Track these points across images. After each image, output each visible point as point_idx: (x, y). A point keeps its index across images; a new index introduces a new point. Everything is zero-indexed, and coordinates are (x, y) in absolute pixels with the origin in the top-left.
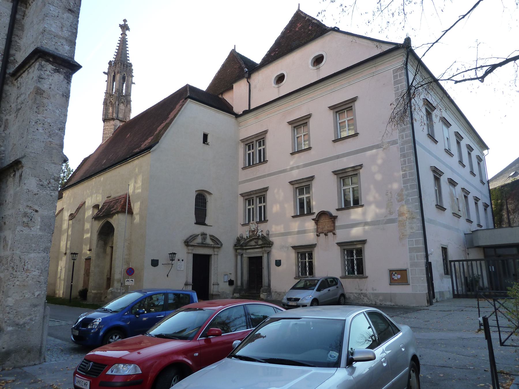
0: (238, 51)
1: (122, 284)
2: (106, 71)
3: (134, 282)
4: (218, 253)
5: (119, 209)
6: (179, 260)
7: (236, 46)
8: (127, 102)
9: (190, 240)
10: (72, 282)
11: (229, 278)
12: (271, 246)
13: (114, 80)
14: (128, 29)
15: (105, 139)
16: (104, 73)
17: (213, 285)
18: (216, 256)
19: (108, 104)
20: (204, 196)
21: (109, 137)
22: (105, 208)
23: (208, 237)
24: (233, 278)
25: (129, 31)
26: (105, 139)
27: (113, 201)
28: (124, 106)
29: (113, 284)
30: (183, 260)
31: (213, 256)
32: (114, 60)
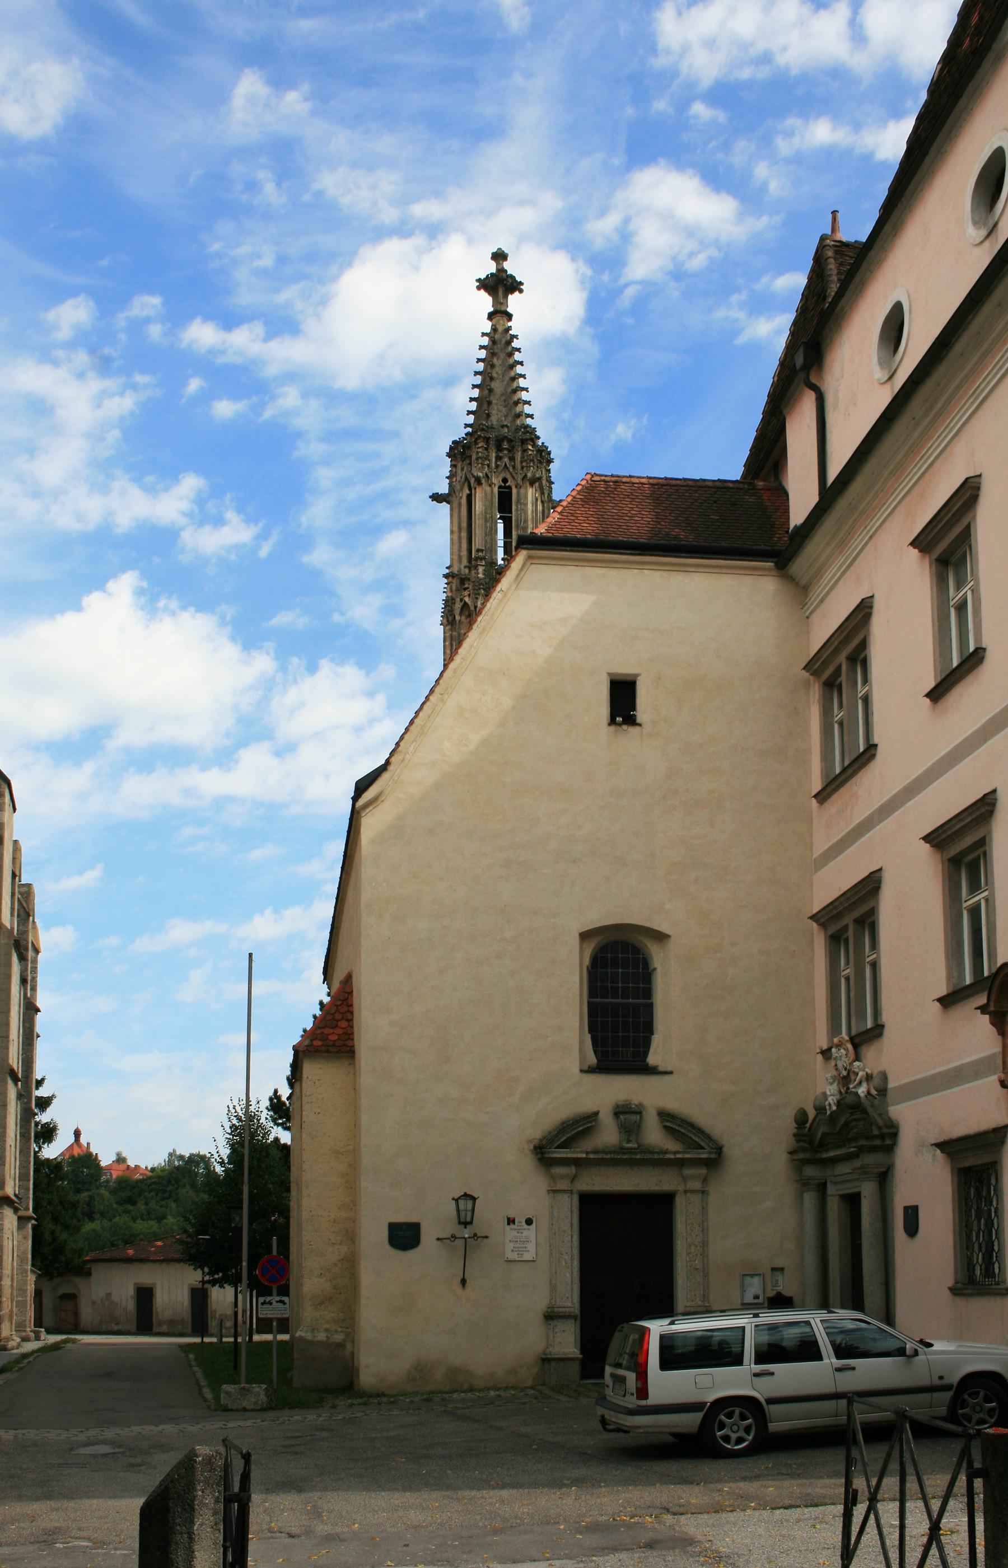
2: (444, 488)
7: (839, 216)
11: (769, 1286)
12: (888, 1142)
16: (437, 498)
19: (457, 618)
30: (529, 1222)
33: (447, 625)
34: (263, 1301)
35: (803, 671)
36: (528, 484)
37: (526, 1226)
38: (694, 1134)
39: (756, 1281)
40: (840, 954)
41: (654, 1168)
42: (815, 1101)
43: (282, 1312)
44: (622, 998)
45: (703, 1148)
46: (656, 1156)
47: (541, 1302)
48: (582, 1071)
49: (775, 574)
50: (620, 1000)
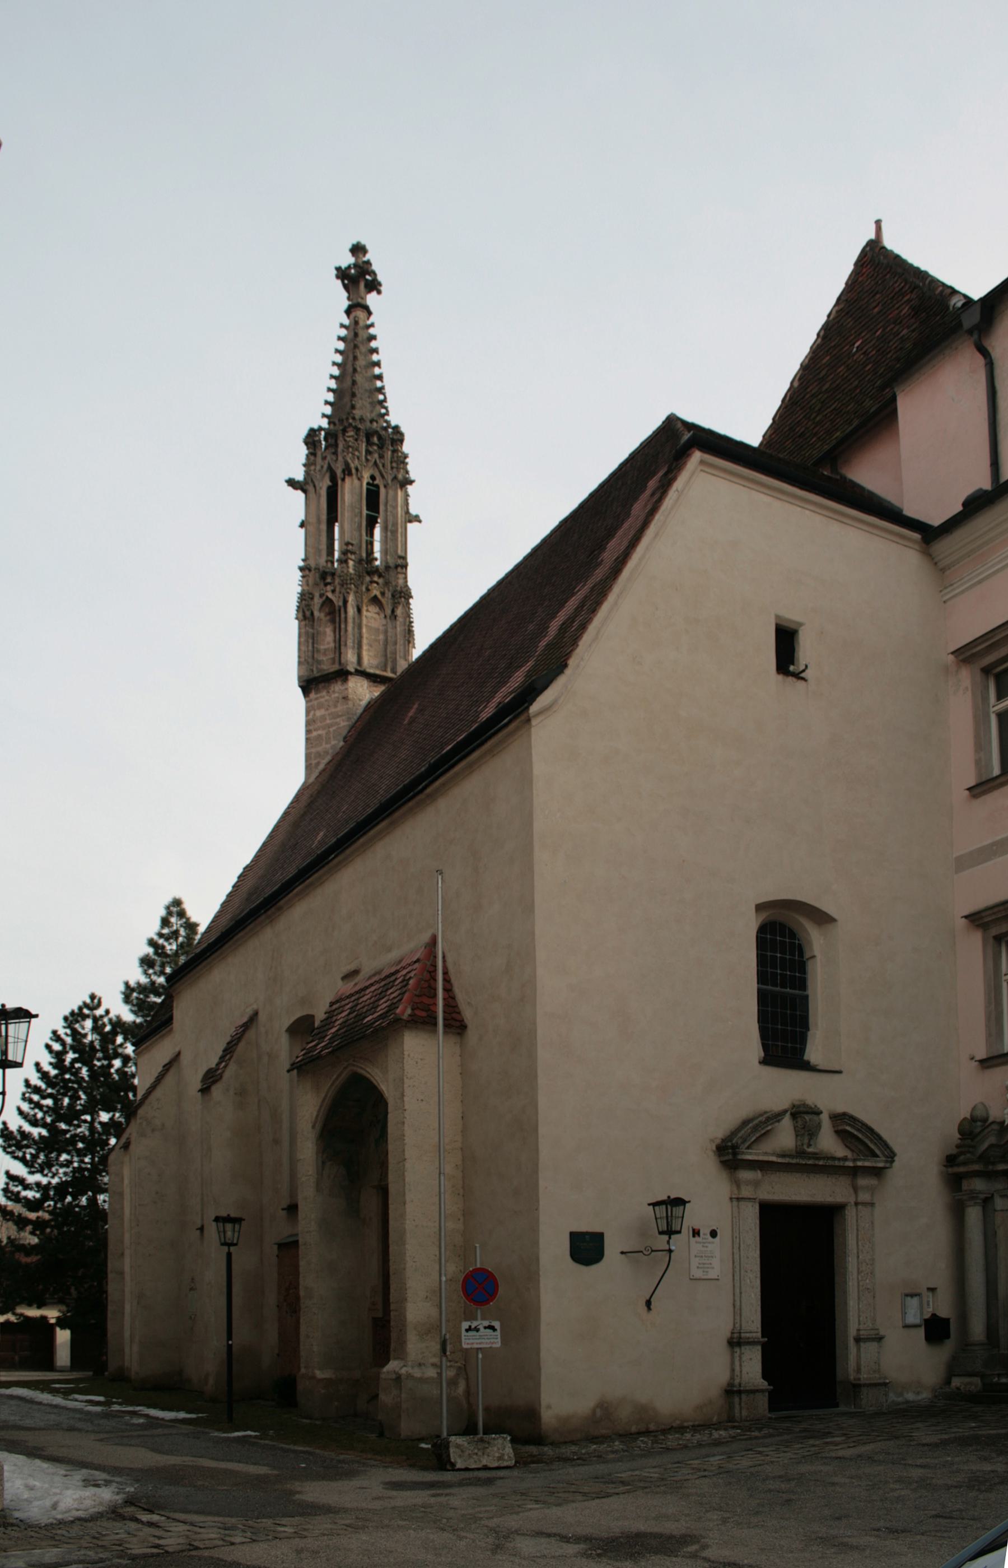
0: (890, 242)
1: (444, 1344)
2: (299, 475)
3: (498, 1333)
4: (872, 1195)
5: (404, 1010)
6: (696, 1233)
7: (884, 226)
8: (393, 596)
9: (744, 1141)
10: (230, 1336)
13: (332, 517)
14: (374, 286)
15: (318, 764)
16: (292, 483)
17: (858, 1340)
18: (864, 1211)
19: (316, 613)
20: (793, 935)
21: (330, 751)
22: (336, 1020)
23: (825, 1118)
24: (944, 1311)
25: (379, 292)
26: (318, 764)
27: (372, 985)
28: (383, 615)
29: (402, 1343)
30: (714, 1234)
31: (850, 1213)
32: (324, 423)
33: (302, 621)
34: (467, 1327)
35: (951, 657)
36: (398, 486)
37: (711, 1239)
38: (871, 1141)
39: (914, 1302)
40: (1001, 957)
41: (828, 1177)
42: (974, 1109)
43: (492, 1341)
44: (781, 987)
45: (875, 1155)
46: (837, 1163)
47: (724, 1328)
48: (760, 1063)
49: (918, 548)
50: (778, 989)
